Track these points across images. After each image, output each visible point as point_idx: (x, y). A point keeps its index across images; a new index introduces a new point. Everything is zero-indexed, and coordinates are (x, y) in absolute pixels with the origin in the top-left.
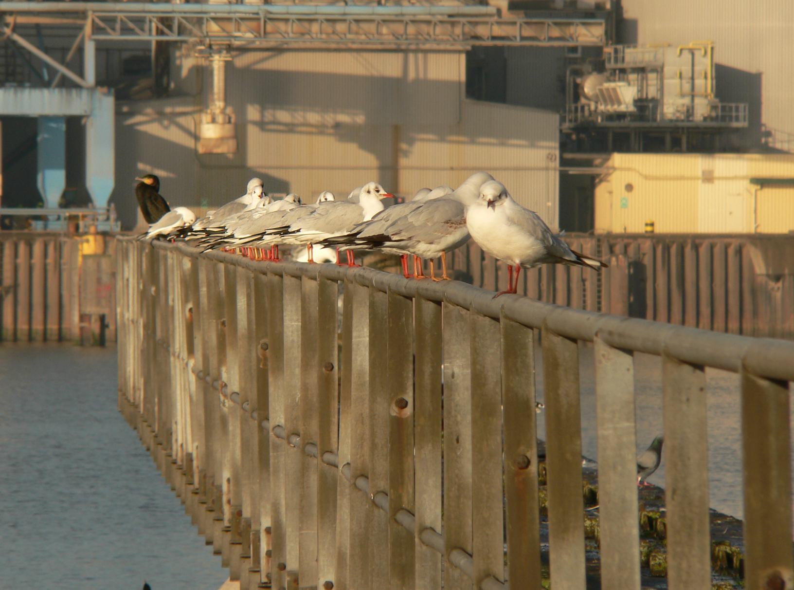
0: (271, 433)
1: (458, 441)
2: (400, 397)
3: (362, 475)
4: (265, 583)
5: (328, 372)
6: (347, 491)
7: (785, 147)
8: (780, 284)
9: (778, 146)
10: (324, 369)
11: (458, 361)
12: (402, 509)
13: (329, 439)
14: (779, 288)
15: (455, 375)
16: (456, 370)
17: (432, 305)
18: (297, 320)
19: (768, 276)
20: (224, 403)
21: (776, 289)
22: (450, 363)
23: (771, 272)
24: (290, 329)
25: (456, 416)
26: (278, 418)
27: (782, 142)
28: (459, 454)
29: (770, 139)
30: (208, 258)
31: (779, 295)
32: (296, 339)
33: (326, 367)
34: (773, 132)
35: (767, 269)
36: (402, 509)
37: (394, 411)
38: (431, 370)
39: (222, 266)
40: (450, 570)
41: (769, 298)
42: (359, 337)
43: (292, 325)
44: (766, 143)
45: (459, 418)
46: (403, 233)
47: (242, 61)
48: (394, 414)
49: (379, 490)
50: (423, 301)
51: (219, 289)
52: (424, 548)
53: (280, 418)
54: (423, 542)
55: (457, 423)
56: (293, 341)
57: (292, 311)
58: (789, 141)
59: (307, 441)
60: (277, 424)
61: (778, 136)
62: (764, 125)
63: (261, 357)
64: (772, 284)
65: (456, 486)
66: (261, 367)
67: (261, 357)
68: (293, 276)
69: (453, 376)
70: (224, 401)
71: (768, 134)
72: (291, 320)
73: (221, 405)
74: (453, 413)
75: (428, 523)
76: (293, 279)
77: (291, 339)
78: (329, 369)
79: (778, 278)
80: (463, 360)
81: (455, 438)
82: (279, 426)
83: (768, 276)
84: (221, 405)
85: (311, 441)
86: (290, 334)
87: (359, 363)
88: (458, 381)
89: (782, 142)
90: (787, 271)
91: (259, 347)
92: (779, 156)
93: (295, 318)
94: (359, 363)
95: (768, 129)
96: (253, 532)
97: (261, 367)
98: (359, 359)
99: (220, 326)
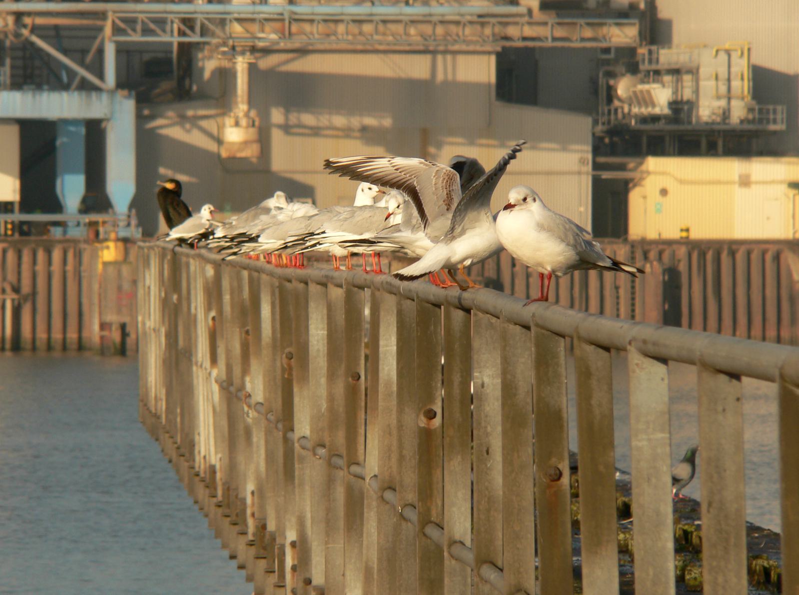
0: (296, 445)
1: (488, 453)
2: (428, 407)
3: (390, 488)
5: (354, 382)
10: (350, 379)
13: (356, 450)
15: (485, 385)
18: (323, 329)
22: (480, 372)
24: (316, 338)
25: (486, 427)
26: (303, 429)
33: (353, 377)
39: (245, 273)
40: (480, 585)
42: (387, 346)
43: (318, 334)
45: (489, 429)
48: (422, 425)
49: (407, 503)
50: (452, 309)
51: (243, 296)
52: (453, 562)
53: (305, 429)
54: (452, 556)
56: (318, 350)
57: (317, 320)
60: (302, 435)
63: (285, 366)
65: (486, 499)
66: (286, 376)
67: (285, 366)
70: (248, 411)
73: (245, 415)
74: (483, 424)
75: (457, 537)
76: (319, 287)
78: (356, 378)
80: (493, 369)
81: (485, 449)
82: (304, 437)
84: (245, 415)
85: (336, 453)
86: (315, 343)
91: (284, 355)
93: (321, 326)
96: (279, 546)
98: (386, 369)
99: (243, 335)
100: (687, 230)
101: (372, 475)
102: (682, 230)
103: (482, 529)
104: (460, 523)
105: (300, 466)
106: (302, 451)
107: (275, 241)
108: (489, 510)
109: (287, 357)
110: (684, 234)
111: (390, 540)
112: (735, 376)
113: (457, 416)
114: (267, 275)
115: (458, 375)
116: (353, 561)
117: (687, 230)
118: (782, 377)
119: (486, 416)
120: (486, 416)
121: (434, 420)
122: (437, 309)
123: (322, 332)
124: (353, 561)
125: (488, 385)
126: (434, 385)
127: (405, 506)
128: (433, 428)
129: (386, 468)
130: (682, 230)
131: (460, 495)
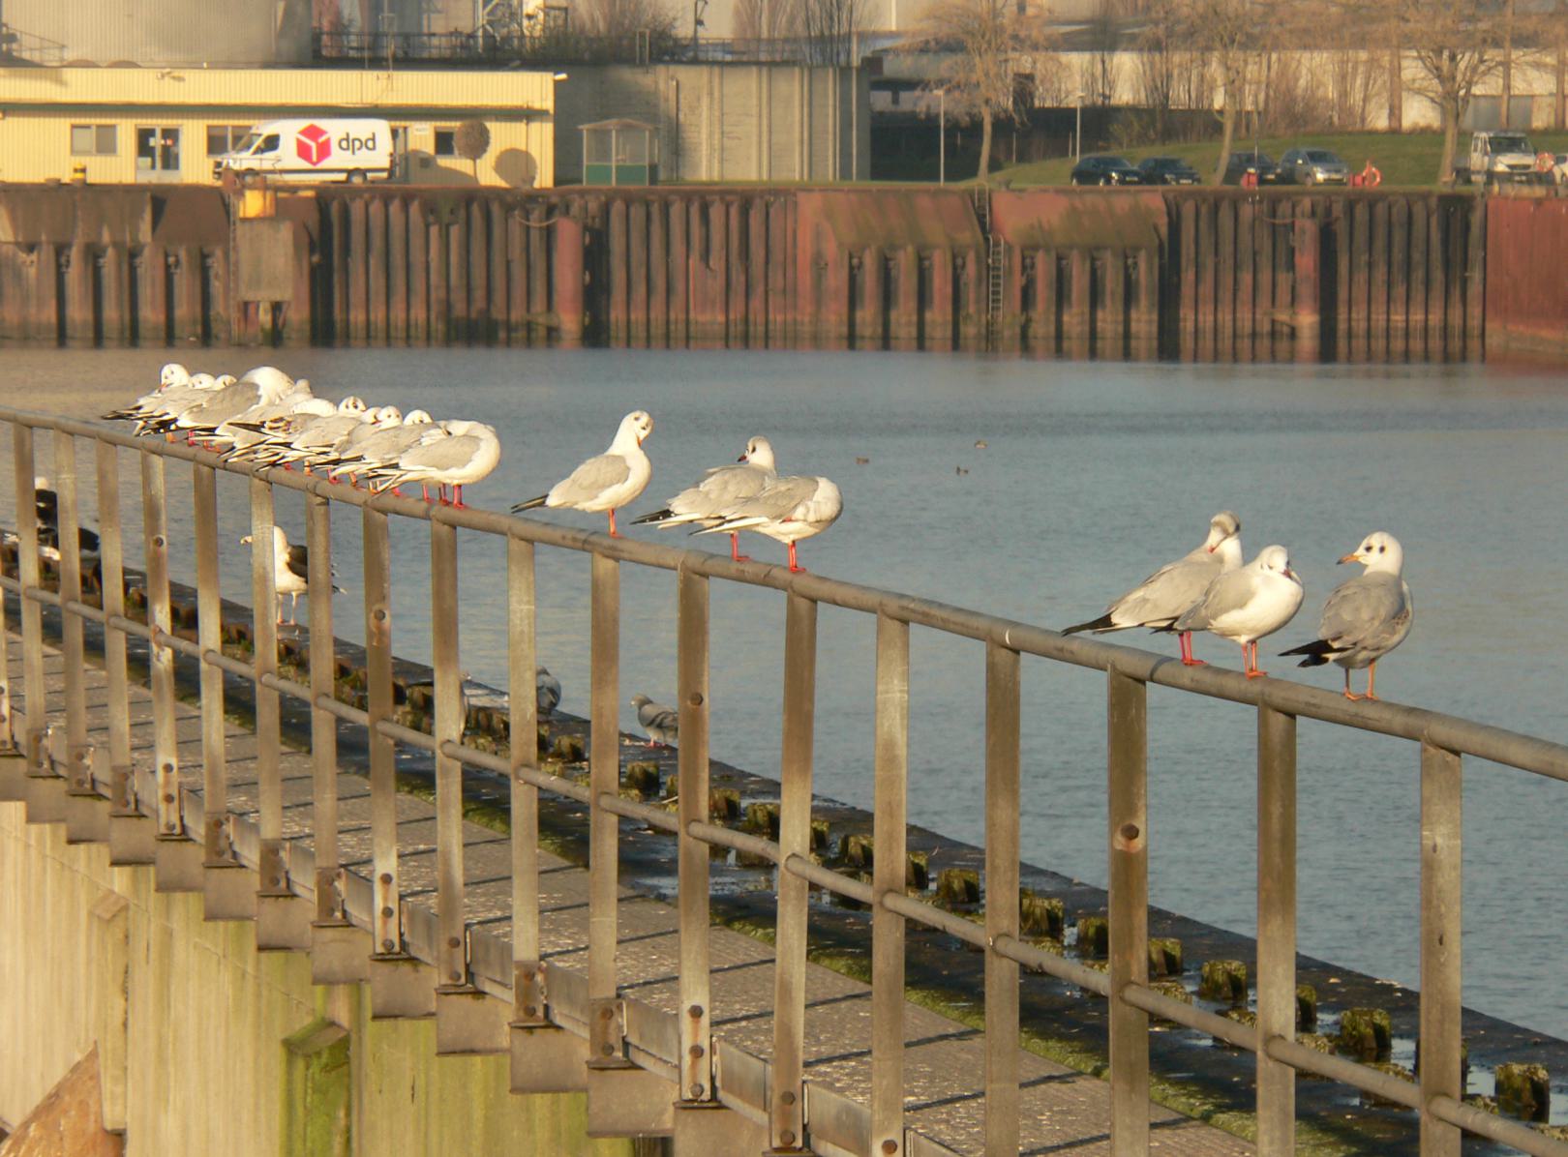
0: (438, 752)
1: (1441, 942)
2: (1127, 823)
3: (891, 890)
4: (382, 954)
6: (792, 894)
7: (36, 57)
8: (34, 257)
9: (26, 55)
10: (689, 703)
11: (1442, 828)
12: (1132, 983)
13: (697, 802)
14: (32, 262)
15: (1439, 848)
16: (1439, 841)
17: (1282, 717)
18: (528, 602)
19: (17, 244)
20: (158, 656)
21: (28, 262)
22: (1431, 830)
23: (20, 239)
24: (518, 615)
25: (1439, 906)
27: (31, 49)
28: (1442, 960)
29: (14, 46)
30: (100, 438)
31: (32, 271)
32: (526, 629)
33: (693, 699)
34: (18, 34)
35: (16, 234)
36: (1132, 983)
37: (1120, 842)
38: (1281, 810)
39: (158, 462)
40: (1430, 1126)
41: (18, 275)
42: (887, 692)
43: (522, 610)
44: (9, 51)
45: (1443, 909)
46: (1345, 638)
47: (281, 195)
48: (1119, 847)
49: (1002, 932)
50: (1270, 712)
52: (1271, 1064)
54: (1269, 1056)
55: (1441, 917)
56: (522, 632)
58: (41, 49)
59: (599, 790)
60: (447, 738)
61: (26, 41)
62: (6, 25)
63: (374, 630)
64: (22, 256)
65: (1439, 1006)
66: (375, 644)
67: (374, 630)
68: (522, 539)
69: (1435, 848)
71: (12, 38)
72: (520, 602)
74: (1435, 902)
75: (1276, 1029)
76: (523, 543)
77: (519, 629)
79: (31, 248)
80: (1450, 826)
81: (1437, 938)
82: (449, 741)
83: (17, 244)
85: (605, 790)
86: (518, 622)
87: (886, 729)
88: (1442, 857)
89: (31, 49)
90: (44, 238)
91: (372, 615)
92: (28, 70)
93: (525, 599)
94: (886, 729)
95: (11, 31)
97: (375, 644)
98: (887, 724)
99: (152, 546)
100: (84, 170)
101: (789, 854)
102: (76, 171)
103: (1434, 1049)
104: (1280, 1010)
105: (444, 781)
106: (445, 759)
107: (421, 468)
108: (1442, 1022)
109: (376, 617)
110: (79, 176)
111: (891, 962)
112: (115, 445)
113: (1277, 860)
114: (261, 479)
115: (1279, 804)
116: (692, 956)
117: (84, 170)
118: (1114, 667)
119: (1440, 892)
120: (1440, 892)
121: (1136, 840)
122: (1140, 686)
123: (527, 607)
124: (692, 956)
125: (1442, 848)
126: (1135, 791)
127: (998, 937)
128: (1134, 851)
129: (885, 864)
130: (76, 171)
131: (1280, 970)
